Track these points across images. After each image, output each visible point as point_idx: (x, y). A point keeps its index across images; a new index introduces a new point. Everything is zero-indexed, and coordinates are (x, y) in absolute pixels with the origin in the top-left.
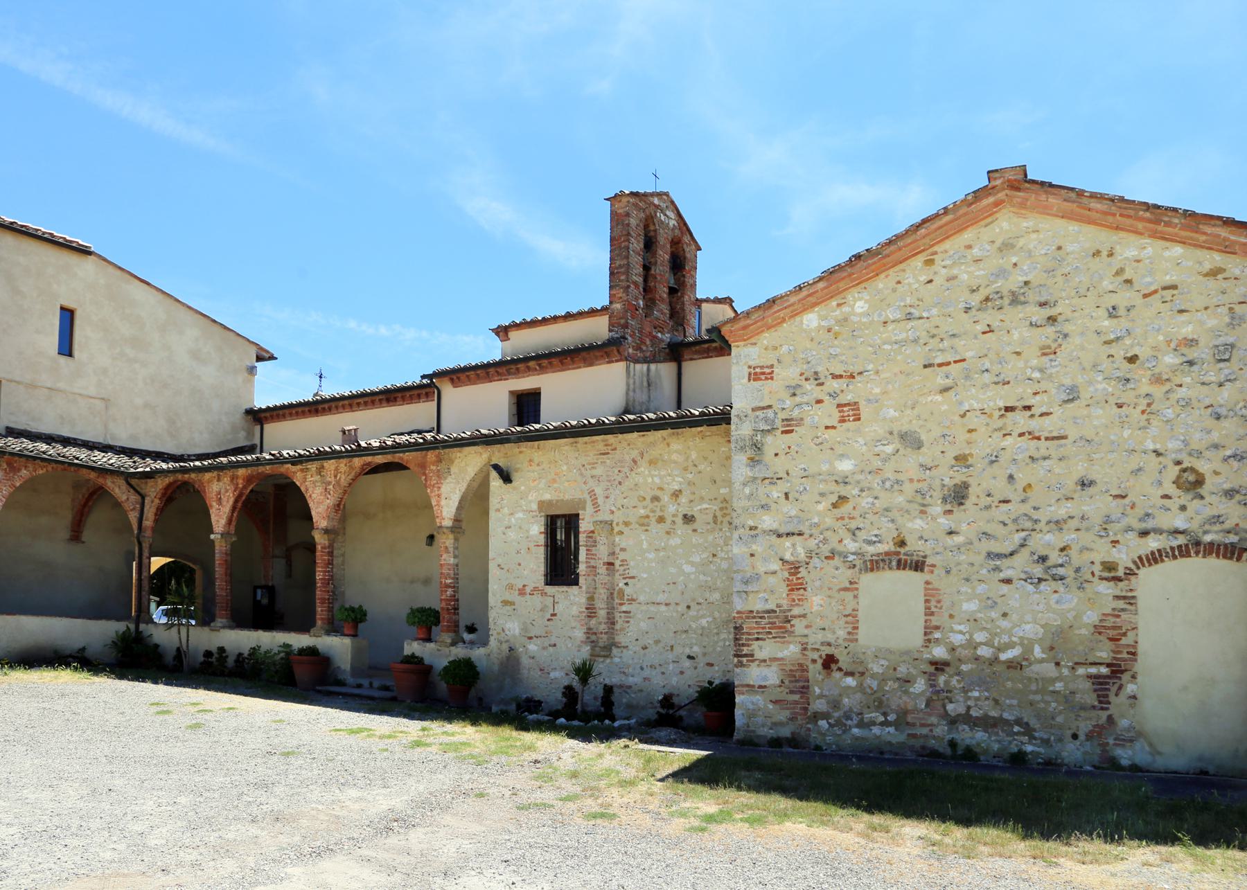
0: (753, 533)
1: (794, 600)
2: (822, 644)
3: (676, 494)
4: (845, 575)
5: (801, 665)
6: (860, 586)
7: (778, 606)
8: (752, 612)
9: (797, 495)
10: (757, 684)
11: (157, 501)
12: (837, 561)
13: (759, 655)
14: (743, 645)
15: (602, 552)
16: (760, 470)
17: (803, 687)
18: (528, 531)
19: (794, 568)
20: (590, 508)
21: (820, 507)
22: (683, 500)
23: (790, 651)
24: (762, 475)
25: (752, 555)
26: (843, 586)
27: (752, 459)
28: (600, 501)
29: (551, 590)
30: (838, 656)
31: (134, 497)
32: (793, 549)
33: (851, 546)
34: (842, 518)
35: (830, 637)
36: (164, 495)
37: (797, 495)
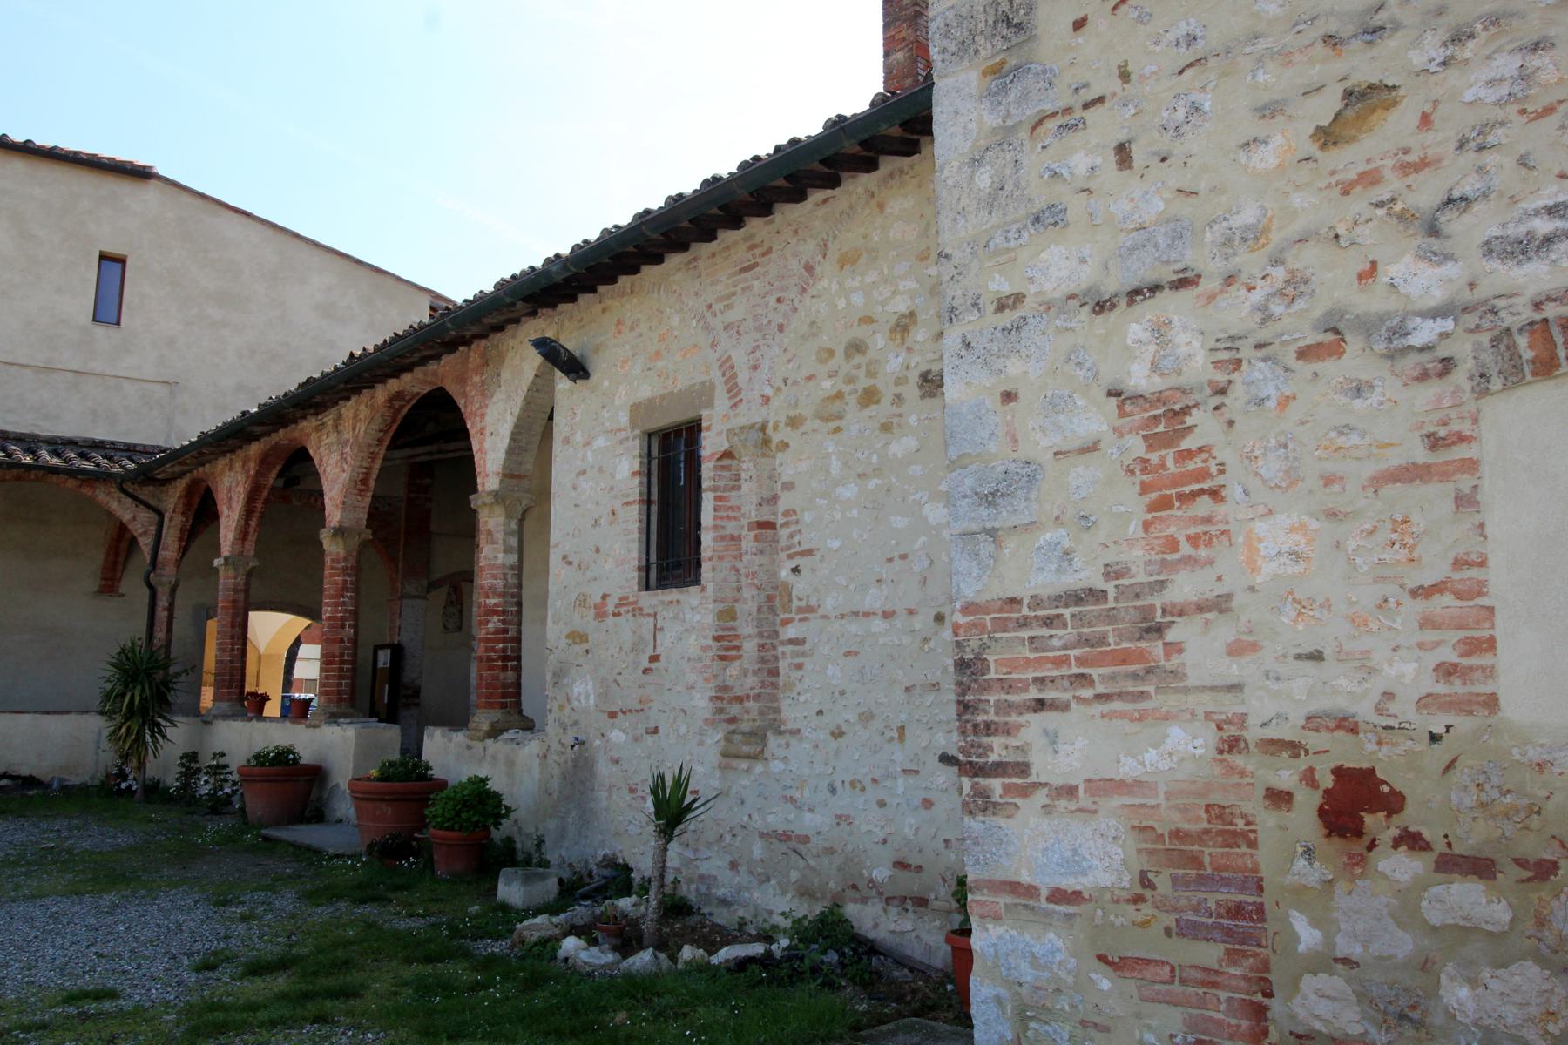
0: (1008, 318)
1: (1172, 545)
2: (1313, 722)
3: (903, 326)
4: (1397, 413)
5: (1218, 813)
6: (1486, 449)
7: (1112, 572)
8: (1014, 602)
9: (1164, 142)
10: (1045, 884)
11: (179, 518)
12: (1355, 361)
13: (1048, 766)
14: (989, 728)
15: (748, 499)
16: (1025, 96)
17: (1237, 911)
18: (613, 476)
19: (1165, 417)
20: (722, 401)
21: (1265, 158)
22: (920, 335)
23: (1174, 751)
24: (1031, 112)
25: (1008, 397)
26: (1394, 459)
27: (996, 71)
28: (743, 378)
29: (650, 600)
30: (1393, 776)
31: (144, 516)
32: (1165, 346)
33: (1418, 279)
34: (1370, 178)
35: (1344, 690)
36: (188, 506)
37: (1164, 142)
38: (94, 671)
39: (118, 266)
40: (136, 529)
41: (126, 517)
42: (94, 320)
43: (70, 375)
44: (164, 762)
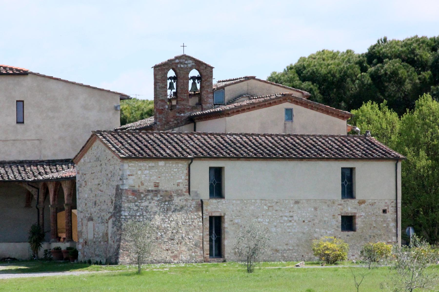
11: (43, 190)
31: (34, 190)
38: (26, 231)
39: (18, 121)
40: (33, 193)
41: (30, 190)
42: (17, 101)
43: (12, 141)
44: (41, 253)
